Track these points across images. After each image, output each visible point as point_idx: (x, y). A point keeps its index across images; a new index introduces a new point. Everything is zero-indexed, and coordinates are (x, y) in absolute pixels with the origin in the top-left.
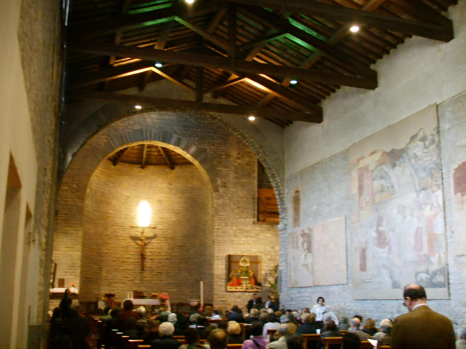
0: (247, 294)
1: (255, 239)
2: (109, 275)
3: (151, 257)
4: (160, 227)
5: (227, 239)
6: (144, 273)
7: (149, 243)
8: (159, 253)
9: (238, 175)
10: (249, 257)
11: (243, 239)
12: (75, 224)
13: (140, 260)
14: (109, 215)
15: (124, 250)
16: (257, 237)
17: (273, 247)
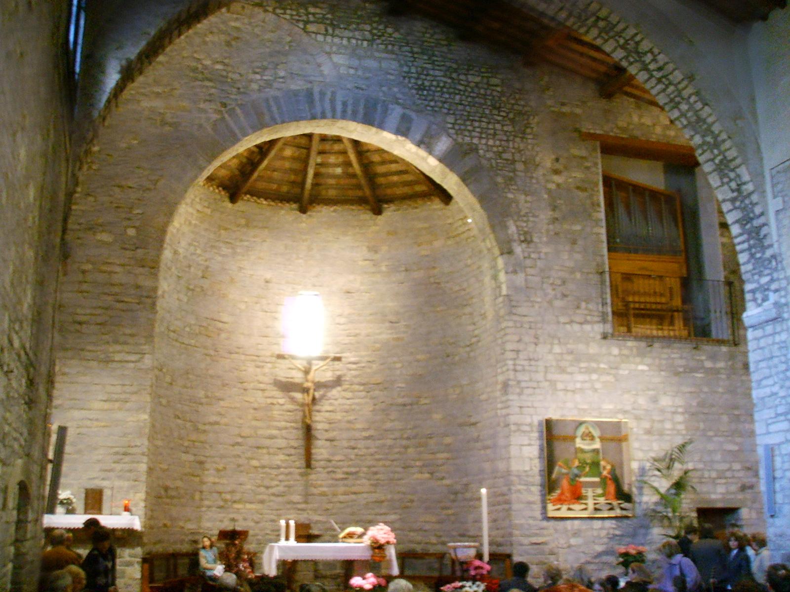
0: (597, 524)
1: (610, 378)
2: (224, 481)
3: (331, 435)
4: (349, 357)
5: (540, 376)
6: (313, 477)
7: (323, 397)
8: (349, 422)
9: (557, 214)
10: (599, 425)
11: (580, 377)
12: (132, 335)
13: (301, 442)
14: (220, 325)
15: (259, 414)
16: (613, 371)
17: (655, 400)
